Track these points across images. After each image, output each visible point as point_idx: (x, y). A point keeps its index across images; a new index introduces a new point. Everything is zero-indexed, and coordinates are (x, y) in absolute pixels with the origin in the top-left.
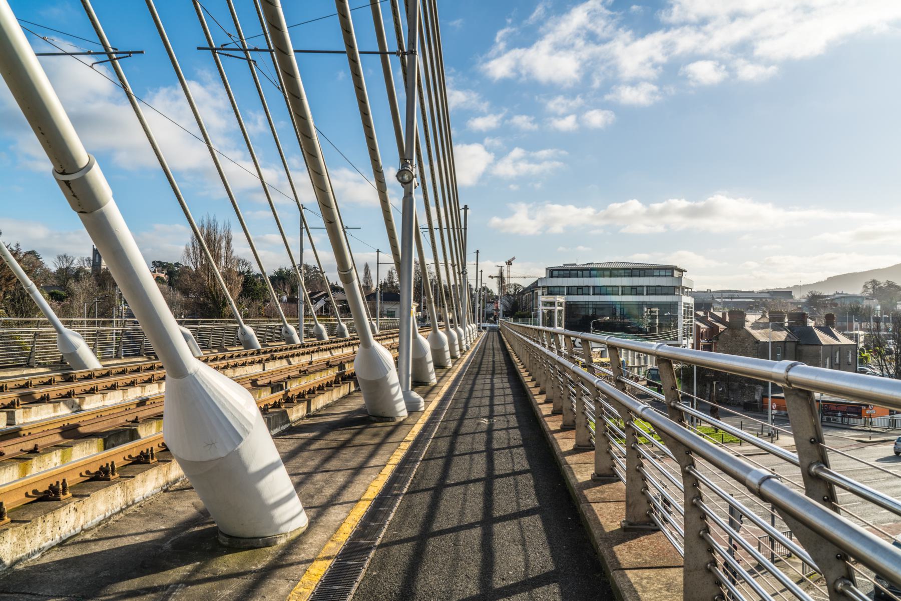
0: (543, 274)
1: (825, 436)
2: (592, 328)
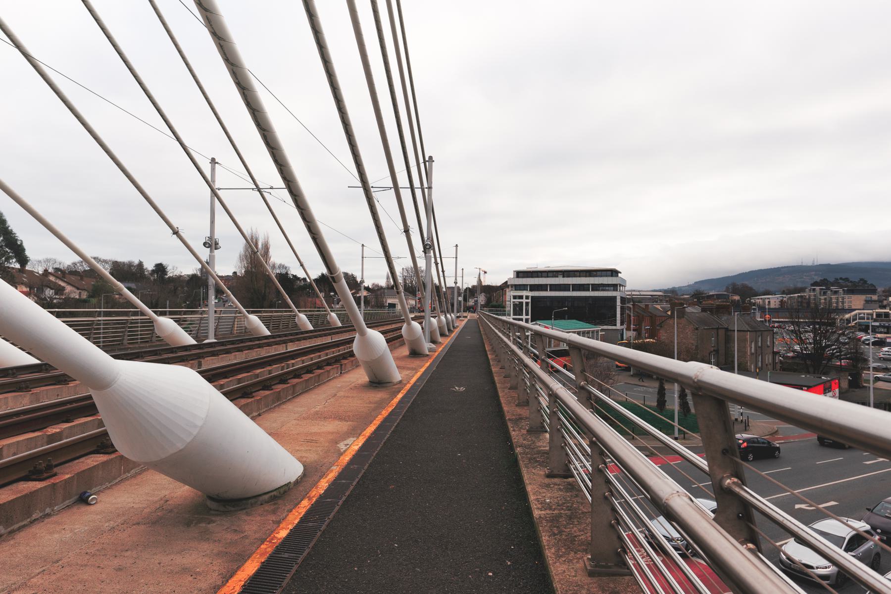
0: (512, 275)
1: (730, 406)
2: (553, 317)
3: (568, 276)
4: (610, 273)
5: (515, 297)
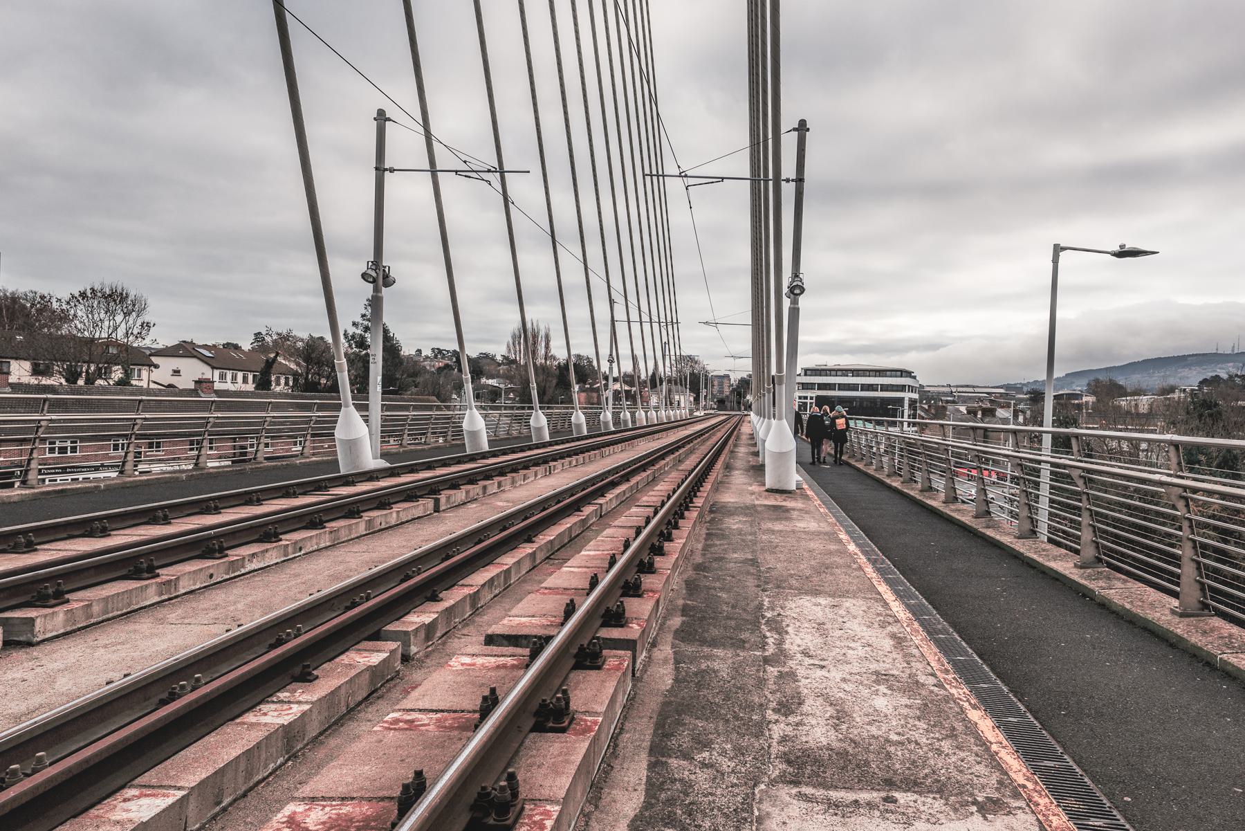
3: (858, 376)
4: (899, 373)
5: (800, 398)
